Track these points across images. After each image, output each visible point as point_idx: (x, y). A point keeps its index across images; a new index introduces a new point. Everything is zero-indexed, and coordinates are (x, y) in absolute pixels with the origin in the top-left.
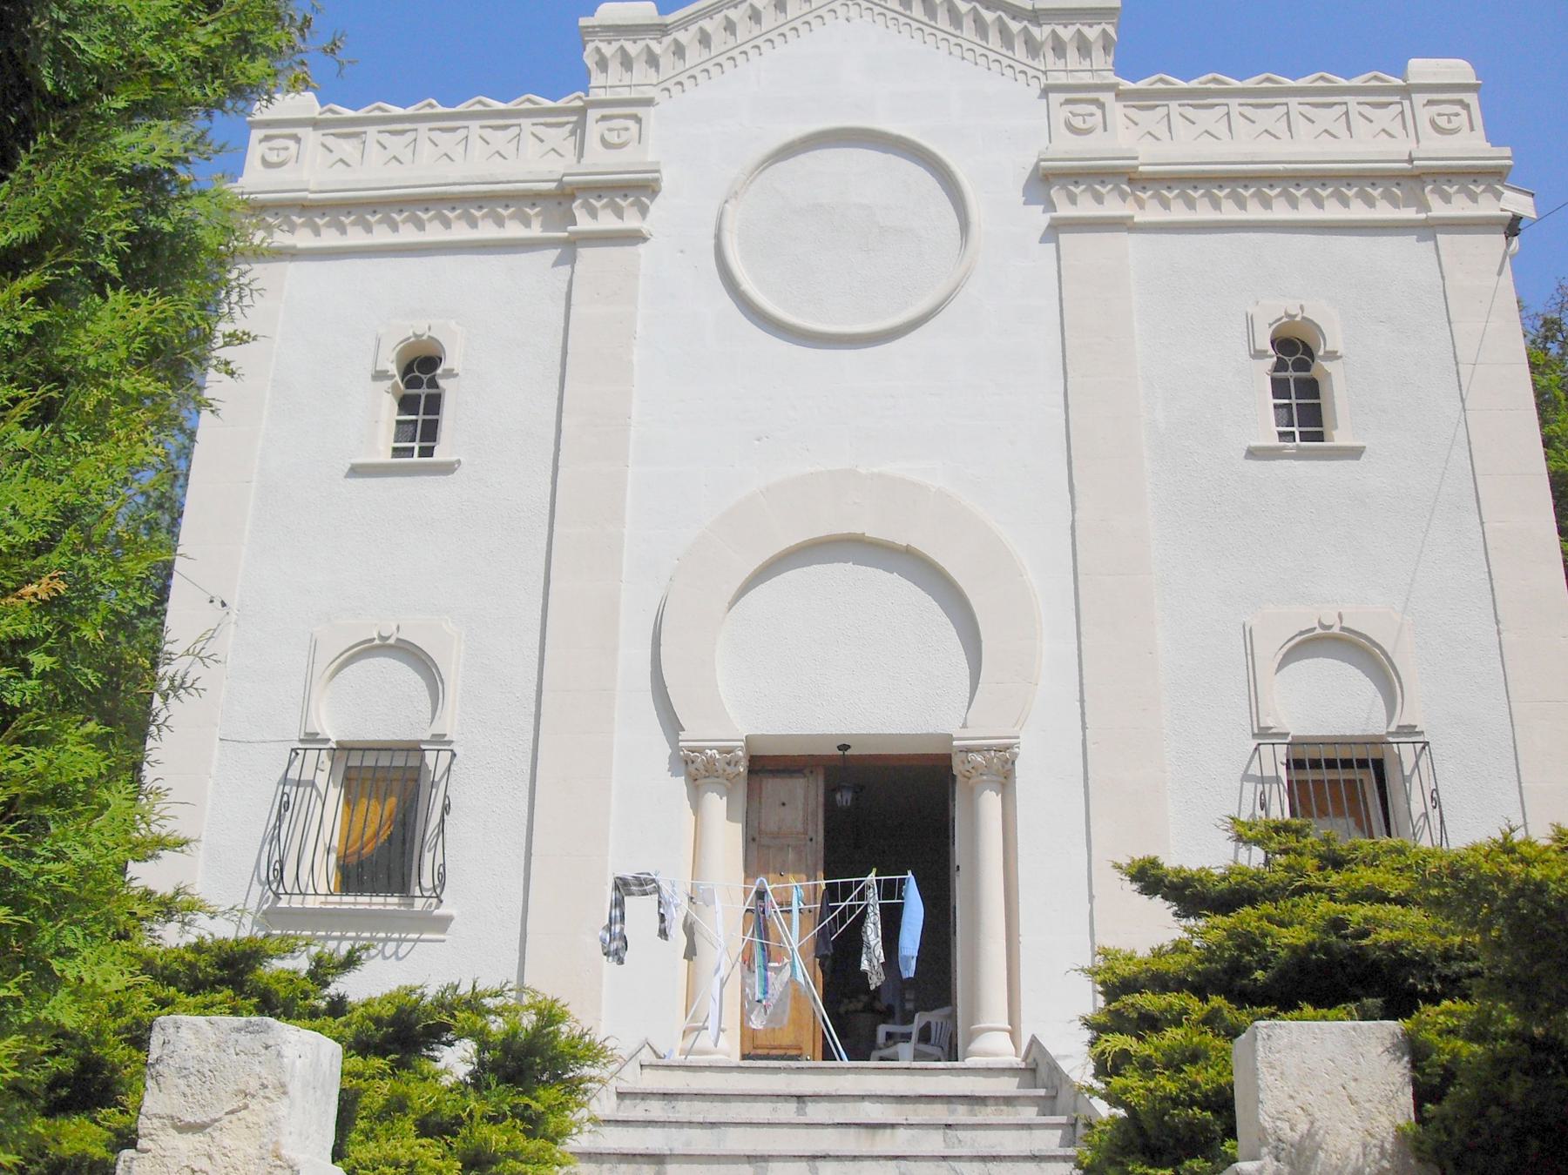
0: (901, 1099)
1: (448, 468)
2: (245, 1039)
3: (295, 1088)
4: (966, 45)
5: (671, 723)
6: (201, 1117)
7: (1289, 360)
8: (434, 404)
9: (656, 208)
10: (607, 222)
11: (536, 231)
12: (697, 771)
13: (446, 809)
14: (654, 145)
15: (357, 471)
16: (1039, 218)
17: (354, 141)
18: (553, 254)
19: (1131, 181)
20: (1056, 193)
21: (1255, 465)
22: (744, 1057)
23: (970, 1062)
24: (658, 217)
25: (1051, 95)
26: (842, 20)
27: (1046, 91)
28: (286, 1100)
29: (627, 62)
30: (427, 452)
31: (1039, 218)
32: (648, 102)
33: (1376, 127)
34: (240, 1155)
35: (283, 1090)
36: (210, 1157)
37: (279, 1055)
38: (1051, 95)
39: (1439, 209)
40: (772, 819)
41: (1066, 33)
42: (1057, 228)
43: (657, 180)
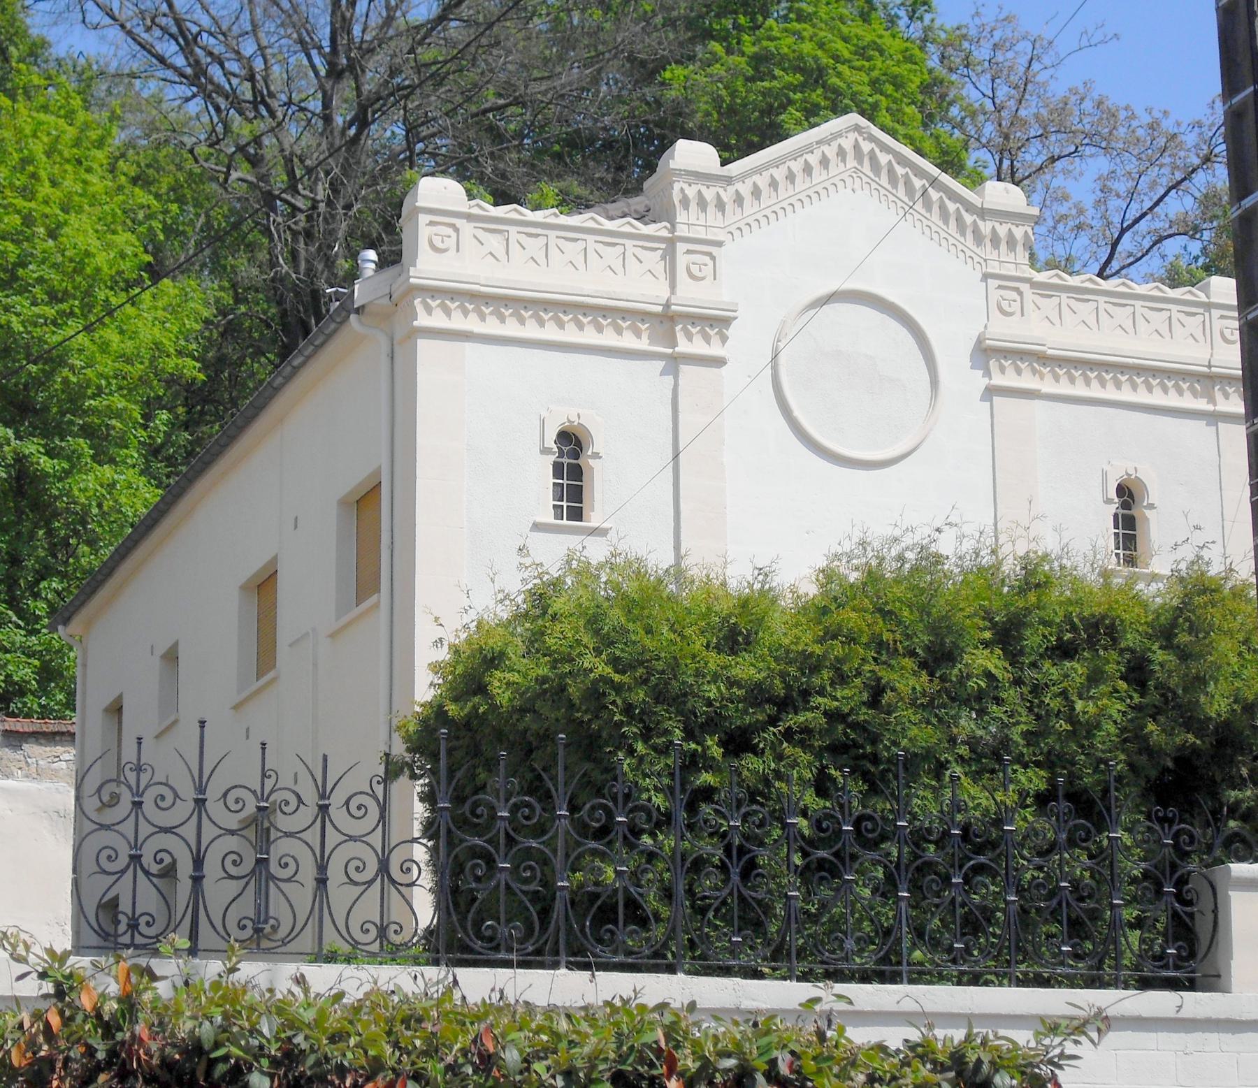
4: (934, 228)
11: (643, 344)
16: (979, 381)
17: (499, 237)
18: (660, 365)
20: (993, 364)
25: (989, 280)
26: (849, 191)
29: (702, 204)
31: (979, 381)
32: (719, 244)
38: (989, 280)
41: (1002, 230)
42: (991, 392)
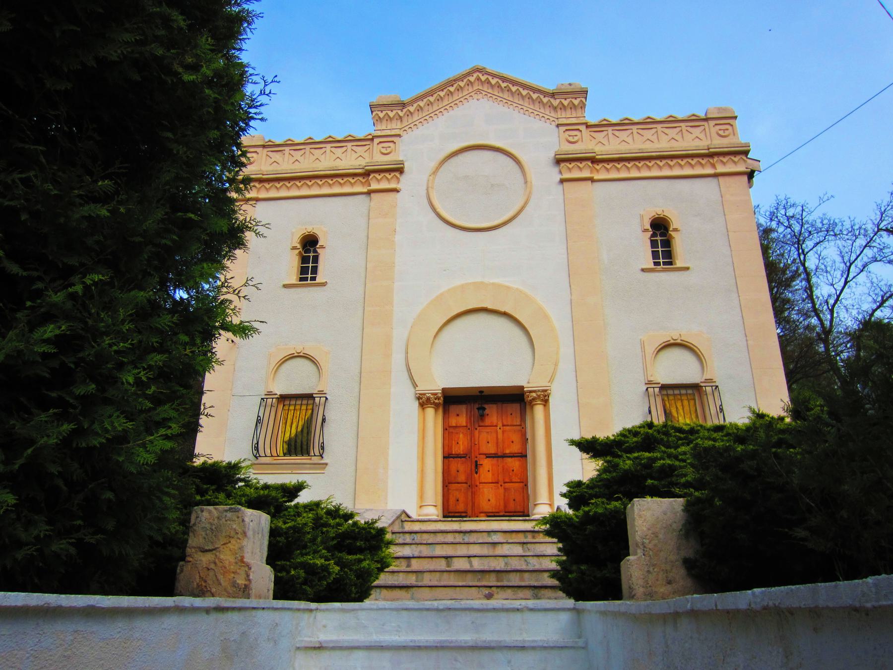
0: (435, 532)
1: (324, 284)
2: (229, 514)
3: (250, 533)
5: (415, 385)
6: (210, 547)
7: (658, 233)
8: (316, 259)
9: (403, 178)
10: (384, 185)
12: (424, 402)
13: (324, 420)
14: (402, 152)
15: (285, 286)
19: (593, 162)
21: (642, 273)
22: (444, 517)
23: (532, 517)
24: (405, 182)
27: (558, 126)
28: (246, 539)
30: (313, 279)
32: (399, 136)
33: (694, 136)
34: (227, 562)
35: (245, 534)
36: (215, 563)
37: (243, 521)
39: (721, 169)
40: (453, 422)
42: (562, 181)
43: (402, 168)
